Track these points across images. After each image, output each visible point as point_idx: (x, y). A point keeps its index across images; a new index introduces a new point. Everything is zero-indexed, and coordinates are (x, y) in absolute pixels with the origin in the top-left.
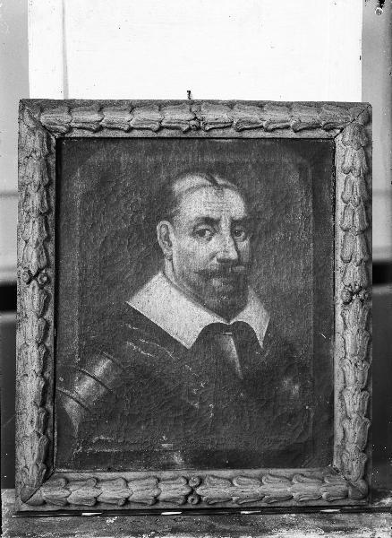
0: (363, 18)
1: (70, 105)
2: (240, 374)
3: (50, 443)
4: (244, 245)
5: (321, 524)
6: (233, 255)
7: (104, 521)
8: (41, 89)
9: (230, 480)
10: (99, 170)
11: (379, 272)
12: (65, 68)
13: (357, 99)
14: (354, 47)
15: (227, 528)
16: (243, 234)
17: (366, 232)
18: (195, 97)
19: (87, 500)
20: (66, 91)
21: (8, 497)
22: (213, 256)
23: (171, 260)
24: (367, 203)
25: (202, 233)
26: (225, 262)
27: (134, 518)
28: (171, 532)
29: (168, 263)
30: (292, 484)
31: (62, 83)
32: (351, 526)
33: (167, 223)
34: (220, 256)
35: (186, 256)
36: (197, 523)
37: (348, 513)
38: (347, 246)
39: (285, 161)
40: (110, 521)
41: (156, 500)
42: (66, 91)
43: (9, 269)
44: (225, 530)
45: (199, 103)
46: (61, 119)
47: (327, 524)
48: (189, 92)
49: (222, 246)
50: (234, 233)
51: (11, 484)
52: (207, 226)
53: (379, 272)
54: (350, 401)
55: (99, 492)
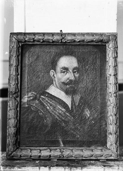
0: (118, 9)
1: (25, 34)
3: (17, 139)
5: (102, 164)
7: (35, 162)
9: (72, 150)
10: (24, 46)
12: (25, 21)
13: (116, 32)
14: (115, 17)
15: (73, 165)
16: (76, 72)
17: (116, 75)
18: (64, 32)
19: (47, 156)
20: (25, 29)
22: (68, 79)
23: (55, 81)
24: (116, 66)
25: (64, 72)
26: (71, 81)
27: (44, 161)
28: (56, 166)
29: (54, 82)
30: (102, 151)
32: (111, 165)
33: (53, 71)
34: (70, 79)
35: (59, 79)
36: (64, 163)
37: (111, 161)
38: (111, 80)
39: (91, 50)
40: (37, 162)
41: (21, 156)
42: (25, 29)
45: (65, 34)
46: (21, 37)
48: (61, 31)
49: (70, 76)
50: (74, 72)
52: (65, 70)
53: (121, 87)
54: (112, 128)
55: (51, 153)
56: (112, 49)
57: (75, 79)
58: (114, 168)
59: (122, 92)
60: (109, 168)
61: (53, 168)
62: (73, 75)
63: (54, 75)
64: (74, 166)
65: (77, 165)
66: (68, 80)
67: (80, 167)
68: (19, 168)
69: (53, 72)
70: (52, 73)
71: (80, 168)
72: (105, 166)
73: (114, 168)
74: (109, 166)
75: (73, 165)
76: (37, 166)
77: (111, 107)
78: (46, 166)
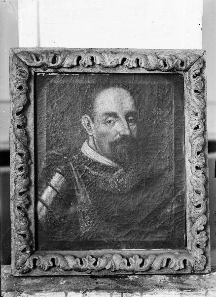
2: (104, 160)
4: (134, 127)
5: (178, 286)
6: (127, 132)
8: (27, 41)
10: (49, 81)
11: (214, 146)
12: (39, 33)
14: (199, 14)
15: (126, 287)
20: (39, 43)
21: (5, 270)
26: (124, 137)
31: (37, 37)
32: (193, 287)
34: (122, 133)
36: (109, 284)
39: (163, 83)
42: (39, 43)
43: (4, 143)
44: (125, 289)
47: (181, 286)
49: (120, 128)
50: (128, 122)
51: (8, 262)
56: (196, 213)
57: (131, 132)
58: (199, 292)
59: (213, 156)
60: (189, 293)
61: (91, 293)
62: (126, 125)
63: (89, 124)
64: (127, 289)
65: (133, 287)
66: (118, 136)
67: (137, 290)
68: (31, 294)
69: (88, 118)
70: (85, 120)
71: (138, 293)
72: (182, 289)
73: (199, 292)
74: (189, 289)
75: (126, 287)
76: (60, 291)
77: (199, 224)
78: (77, 291)
